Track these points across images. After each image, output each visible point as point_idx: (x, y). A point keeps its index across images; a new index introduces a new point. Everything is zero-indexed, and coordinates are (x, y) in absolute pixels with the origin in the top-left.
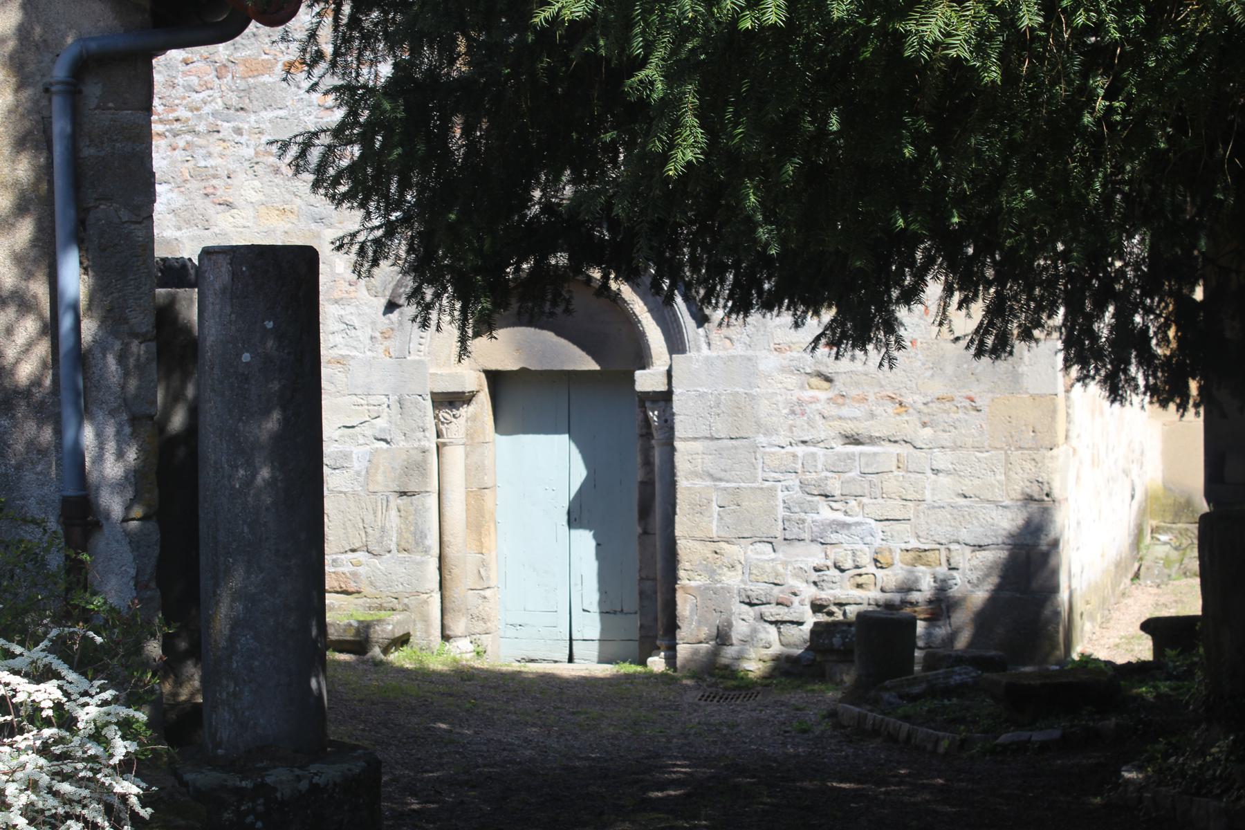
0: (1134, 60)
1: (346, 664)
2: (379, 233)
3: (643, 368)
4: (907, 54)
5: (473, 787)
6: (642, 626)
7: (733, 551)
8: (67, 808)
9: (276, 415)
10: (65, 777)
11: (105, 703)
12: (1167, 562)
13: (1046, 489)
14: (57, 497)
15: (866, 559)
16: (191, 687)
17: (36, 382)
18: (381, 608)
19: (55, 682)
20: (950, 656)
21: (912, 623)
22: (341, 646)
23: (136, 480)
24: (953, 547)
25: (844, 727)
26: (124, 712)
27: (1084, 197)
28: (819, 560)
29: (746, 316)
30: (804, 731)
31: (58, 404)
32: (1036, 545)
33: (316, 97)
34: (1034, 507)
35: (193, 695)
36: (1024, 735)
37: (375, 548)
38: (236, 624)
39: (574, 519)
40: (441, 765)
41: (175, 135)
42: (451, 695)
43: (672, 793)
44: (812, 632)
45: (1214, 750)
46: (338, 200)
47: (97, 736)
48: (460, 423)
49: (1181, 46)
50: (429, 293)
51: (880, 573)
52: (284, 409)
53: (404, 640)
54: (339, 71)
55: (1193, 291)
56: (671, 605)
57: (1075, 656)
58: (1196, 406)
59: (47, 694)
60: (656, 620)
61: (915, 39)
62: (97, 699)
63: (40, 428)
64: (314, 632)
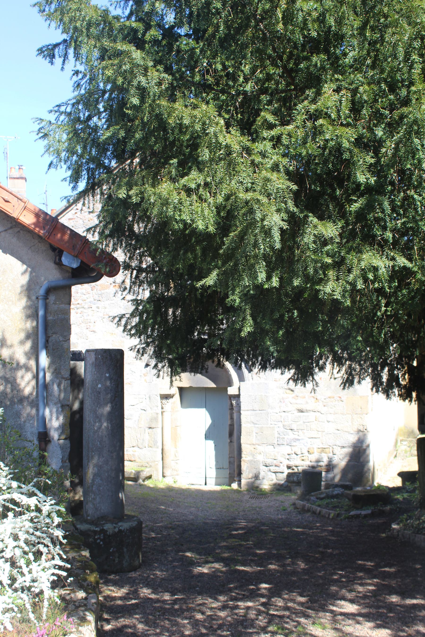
1: (131, 485)
2: (144, 346)
3: (231, 386)
4: (320, 297)
5: (173, 529)
6: (230, 473)
7: (260, 448)
8: (39, 540)
9: (109, 405)
11: (52, 505)
12: (406, 452)
13: (365, 428)
14: (37, 432)
15: (305, 451)
16: (79, 495)
17: (31, 394)
18: (142, 466)
19: (35, 498)
20: (333, 484)
21: (321, 473)
22: (129, 479)
23: (62, 427)
24: (334, 447)
25: (298, 509)
26: (58, 508)
27: (378, 339)
28: (290, 452)
29: (265, 371)
30: (284, 510)
31: (38, 401)
32: (362, 447)
33: (125, 302)
34: (361, 433)
35: (80, 497)
36: (358, 512)
37: (141, 446)
38: (95, 475)
39: (207, 437)
40: (162, 521)
41: (77, 309)
42: (165, 496)
43: (240, 532)
44: (287, 476)
45: (423, 518)
46: (132, 336)
47: (49, 516)
48: (170, 404)
49: (409, 293)
50: (160, 365)
51: (309, 455)
52: (112, 403)
53: (150, 477)
54: (132, 294)
55: (413, 363)
56: (239, 466)
57: (376, 484)
58: (415, 401)
59: (32, 502)
60: (234, 471)
61: (322, 292)
62: (49, 504)
63: (32, 409)
64: (121, 478)
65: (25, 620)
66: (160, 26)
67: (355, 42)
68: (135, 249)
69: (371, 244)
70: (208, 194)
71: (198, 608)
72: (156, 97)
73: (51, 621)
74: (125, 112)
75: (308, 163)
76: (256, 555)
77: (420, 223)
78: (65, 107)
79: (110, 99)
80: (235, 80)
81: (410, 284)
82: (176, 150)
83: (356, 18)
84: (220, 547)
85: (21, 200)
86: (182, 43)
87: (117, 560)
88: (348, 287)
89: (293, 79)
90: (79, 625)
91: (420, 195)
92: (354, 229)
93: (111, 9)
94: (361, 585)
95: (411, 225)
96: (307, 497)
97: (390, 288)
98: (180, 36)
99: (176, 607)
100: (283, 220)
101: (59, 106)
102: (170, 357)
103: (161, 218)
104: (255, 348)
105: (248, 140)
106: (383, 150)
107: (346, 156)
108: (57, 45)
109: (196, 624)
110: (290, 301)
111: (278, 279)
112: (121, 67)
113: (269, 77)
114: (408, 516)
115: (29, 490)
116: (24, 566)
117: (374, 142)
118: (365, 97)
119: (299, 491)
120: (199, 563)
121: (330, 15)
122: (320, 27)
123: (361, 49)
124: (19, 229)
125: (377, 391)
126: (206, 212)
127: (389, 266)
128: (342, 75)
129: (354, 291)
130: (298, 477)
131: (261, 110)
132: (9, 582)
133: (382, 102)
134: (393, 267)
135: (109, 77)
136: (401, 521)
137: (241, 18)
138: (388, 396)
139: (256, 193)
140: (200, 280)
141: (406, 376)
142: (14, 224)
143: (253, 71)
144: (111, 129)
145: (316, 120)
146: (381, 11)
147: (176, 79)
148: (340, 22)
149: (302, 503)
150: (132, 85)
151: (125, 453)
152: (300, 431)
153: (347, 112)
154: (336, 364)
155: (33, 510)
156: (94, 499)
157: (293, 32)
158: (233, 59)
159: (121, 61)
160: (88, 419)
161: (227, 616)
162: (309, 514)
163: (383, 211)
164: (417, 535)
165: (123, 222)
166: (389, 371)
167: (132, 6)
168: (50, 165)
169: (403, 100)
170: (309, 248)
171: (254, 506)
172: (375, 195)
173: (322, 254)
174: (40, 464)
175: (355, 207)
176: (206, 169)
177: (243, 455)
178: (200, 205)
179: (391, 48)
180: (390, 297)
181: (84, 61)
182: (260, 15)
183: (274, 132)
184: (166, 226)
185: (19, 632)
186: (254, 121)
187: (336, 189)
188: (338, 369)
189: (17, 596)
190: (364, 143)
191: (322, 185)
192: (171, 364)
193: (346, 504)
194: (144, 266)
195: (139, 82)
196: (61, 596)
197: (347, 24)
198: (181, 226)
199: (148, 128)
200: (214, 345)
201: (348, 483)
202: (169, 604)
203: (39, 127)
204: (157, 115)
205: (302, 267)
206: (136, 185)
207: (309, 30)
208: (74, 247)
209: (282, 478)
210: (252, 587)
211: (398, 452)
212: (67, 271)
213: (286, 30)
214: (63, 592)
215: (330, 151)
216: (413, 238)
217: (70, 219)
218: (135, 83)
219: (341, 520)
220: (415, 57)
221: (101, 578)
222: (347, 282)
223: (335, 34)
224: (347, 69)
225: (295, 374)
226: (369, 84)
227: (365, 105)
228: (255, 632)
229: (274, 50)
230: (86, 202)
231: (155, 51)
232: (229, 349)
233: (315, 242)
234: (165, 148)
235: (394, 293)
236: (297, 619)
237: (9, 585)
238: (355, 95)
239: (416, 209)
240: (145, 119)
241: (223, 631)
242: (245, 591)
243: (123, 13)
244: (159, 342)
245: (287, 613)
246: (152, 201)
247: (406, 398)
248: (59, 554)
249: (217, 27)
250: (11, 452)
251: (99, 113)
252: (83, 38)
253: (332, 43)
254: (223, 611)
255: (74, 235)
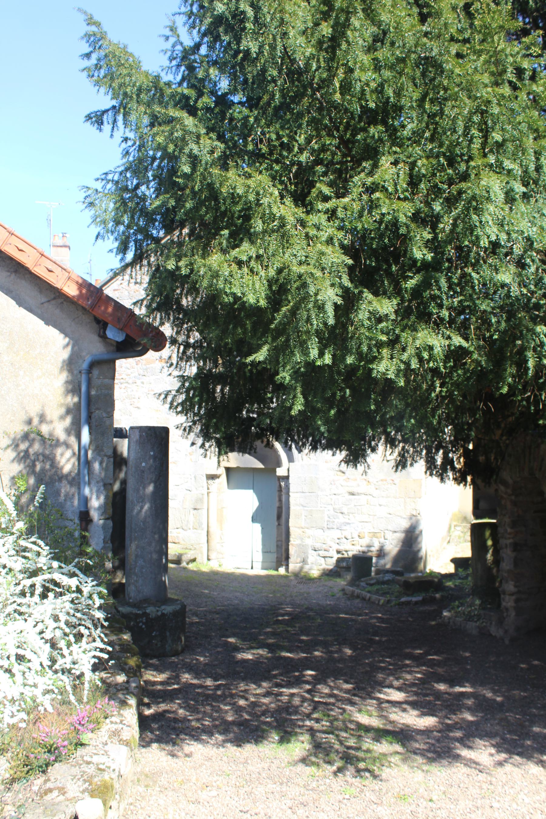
0: (449, 375)
1: (174, 568)
2: (191, 424)
5: (218, 614)
6: (277, 558)
7: (309, 532)
10: (78, 611)
11: (93, 586)
12: (460, 537)
14: (78, 511)
16: (120, 578)
17: (70, 472)
18: (186, 549)
19: (76, 578)
21: (371, 558)
22: (173, 562)
23: (103, 509)
24: (386, 532)
30: (333, 596)
33: (171, 377)
34: (414, 518)
36: (409, 599)
37: (185, 528)
46: (177, 413)
49: (465, 373)
50: (207, 445)
51: (360, 540)
52: (155, 483)
53: (194, 560)
57: (428, 571)
58: (470, 485)
59: (73, 582)
64: (164, 561)
65: (65, 702)
66: (213, 93)
67: (414, 115)
68: (183, 323)
69: (427, 322)
70: (260, 267)
71: (241, 694)
72: (209, 166)
73: (92, 704)
74: (175, 181)
75: (363, 237)
76: (302, 641)
77: (477, 302)
78: (112, 175)
79: (159, 166)
80: (290, 149)
81: (465, 363)
82: (228, 221)
83: (416, 90)
84: (266, 633)
85: (65, 270)
86: (235, 111)
87: (159, 644)
88: (402, 367)
89: (350, 150)
90: (120, 708)
91: (478, 273)
92: (409, 307)
93: (163, 74)
94: (410, 672)
95: (468, 303)
96: (357, 583)
97: (445, 368)
98: (233, 103)
99: (219, 693)
100: (337, 295)
101: (106, 174)
102: (218, 436)
103: (211, 291)
104: (306, 428)
105: (303, 212)
106: (441, 226)
107: (403, 230)
108: (106, 111)
109: (238, 710)
110: (342, 380)
111: (330, 356)
112: (172, 134)
113: (324, 149)
114: (459, 603)
115: (69, 571)
116: (65, 648)
117: (432, 216)
118: (423, 171)
119: (349, 577)
120: (242, 648)
121: (389, 86)
122: (378, 98)
123: (420, 122)
124: (62, 300)
125: (431, 475)
126: (257, 286)
127: (445, 346)
128: (400, 148)
129: (408, 371)
130: (347, 562)
131: (316, 182)
132: (49, 663)
133: (440, 176)
134: (449, 346)
135: (159, 144)
136: (453, 608)
137: (297, 86)
138: (442, 480)
139: (311, 266)
140: (250, 355)
141: (462, 460)
142: (58, 294)
143: (308, 141)
144: (161, 197)
145: (372, 193)
146: (441, 83)
147: (228, 148)
148: (399, 93)
149: (351, 588)
150: (184, 153)
151: (169, 535)
152: (351, 515)
153: (405, 186)
154: (388, 446)
155: (74, 592)
156: (136, 581)
157: (350, 102)
158: (288, 129)
159: (173, 128)
160: (131, 498)
161: (271, 703)
162: (358, 601)
163: (439, 289)
164: (469, 623)
165: (171, 295)
166: (444, 453)
167: (184, 71)
168: (97, 237)
169: (462, 175)
170: (363, 325)
171: (302, 591)
172: (432, 271)
173: (377, 331)
174: (81, 544)
175: (411, 283)
176: (259, 241)
177: (291, 539)
178: (251, 278)
179: (450, 122)
180: (445, 378)
181: (133, 128)
182: (317, 84)
183: (329, 205)
184: (215, 300)
185: (59, 714)
186: (309, 193)
187: (391, 265)
188: (391, 451)
189: (58, 677)
190: (421, 218)
191: (377, 261)
192: (219, 444)
193: (396, 590)
194: (192, 341)
195: (191, 150)
196: (102, 679)
197: (405, 96)
198: (231, 300)
199: (199, 198)
200: (263, 424)
201: (399, 569)
202: (212, 690)
203: (85, 195)
204: (209, 185)
205: (356, 344)
206: (186, 256)
207: (367, 101)
208: (119, 320)
209: (330, 564)
210: (297, 674)
211: (452, 537)
212: (112, 345)
213: (343, 100)
214: (104, 675)
215: (387, 226)
216: (470, 317)
217: (115, 290)
218: (187, 151)
219: (391, 606)
220: (474, 132)
221: (143, 662)
222: (401, 361)
223: (393, 105)
224: (405, 141)
225: (347, 455)
226: (428, 158)
227: (423, 179)
228: (300, 719)
229: (331, 119)
230: (134, 274)
231: (208, 118)
232: (278, 428)
233: (369, 319)
234: (215, 218)
235: (449, 373)
236: (344, 706)
237: (49, 666)
238: (413, 169)
239: (473, 287)
240: (196, 189)
241: (267, 718)
242: (290, 678)
243: (175, 79)
244: (206, 420)
245: (332, 700)
246: (202, 273)
247: (461, 482)
248: (100, 637)
249: (273, 96)
250: (52, 532)
251: (149, 182)
252: (133, 105)
253: (390, 114)
254: (267, 697)
255: (119, 306)
